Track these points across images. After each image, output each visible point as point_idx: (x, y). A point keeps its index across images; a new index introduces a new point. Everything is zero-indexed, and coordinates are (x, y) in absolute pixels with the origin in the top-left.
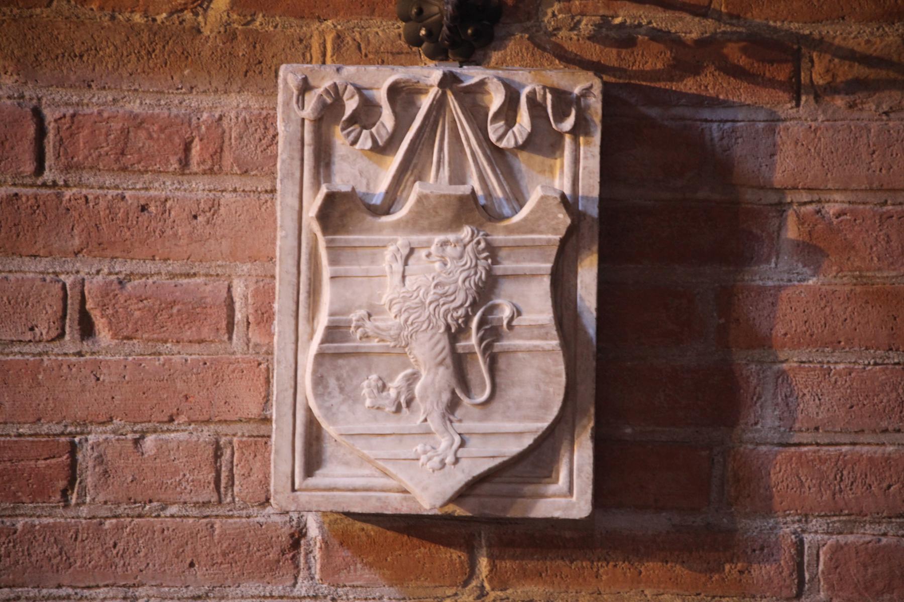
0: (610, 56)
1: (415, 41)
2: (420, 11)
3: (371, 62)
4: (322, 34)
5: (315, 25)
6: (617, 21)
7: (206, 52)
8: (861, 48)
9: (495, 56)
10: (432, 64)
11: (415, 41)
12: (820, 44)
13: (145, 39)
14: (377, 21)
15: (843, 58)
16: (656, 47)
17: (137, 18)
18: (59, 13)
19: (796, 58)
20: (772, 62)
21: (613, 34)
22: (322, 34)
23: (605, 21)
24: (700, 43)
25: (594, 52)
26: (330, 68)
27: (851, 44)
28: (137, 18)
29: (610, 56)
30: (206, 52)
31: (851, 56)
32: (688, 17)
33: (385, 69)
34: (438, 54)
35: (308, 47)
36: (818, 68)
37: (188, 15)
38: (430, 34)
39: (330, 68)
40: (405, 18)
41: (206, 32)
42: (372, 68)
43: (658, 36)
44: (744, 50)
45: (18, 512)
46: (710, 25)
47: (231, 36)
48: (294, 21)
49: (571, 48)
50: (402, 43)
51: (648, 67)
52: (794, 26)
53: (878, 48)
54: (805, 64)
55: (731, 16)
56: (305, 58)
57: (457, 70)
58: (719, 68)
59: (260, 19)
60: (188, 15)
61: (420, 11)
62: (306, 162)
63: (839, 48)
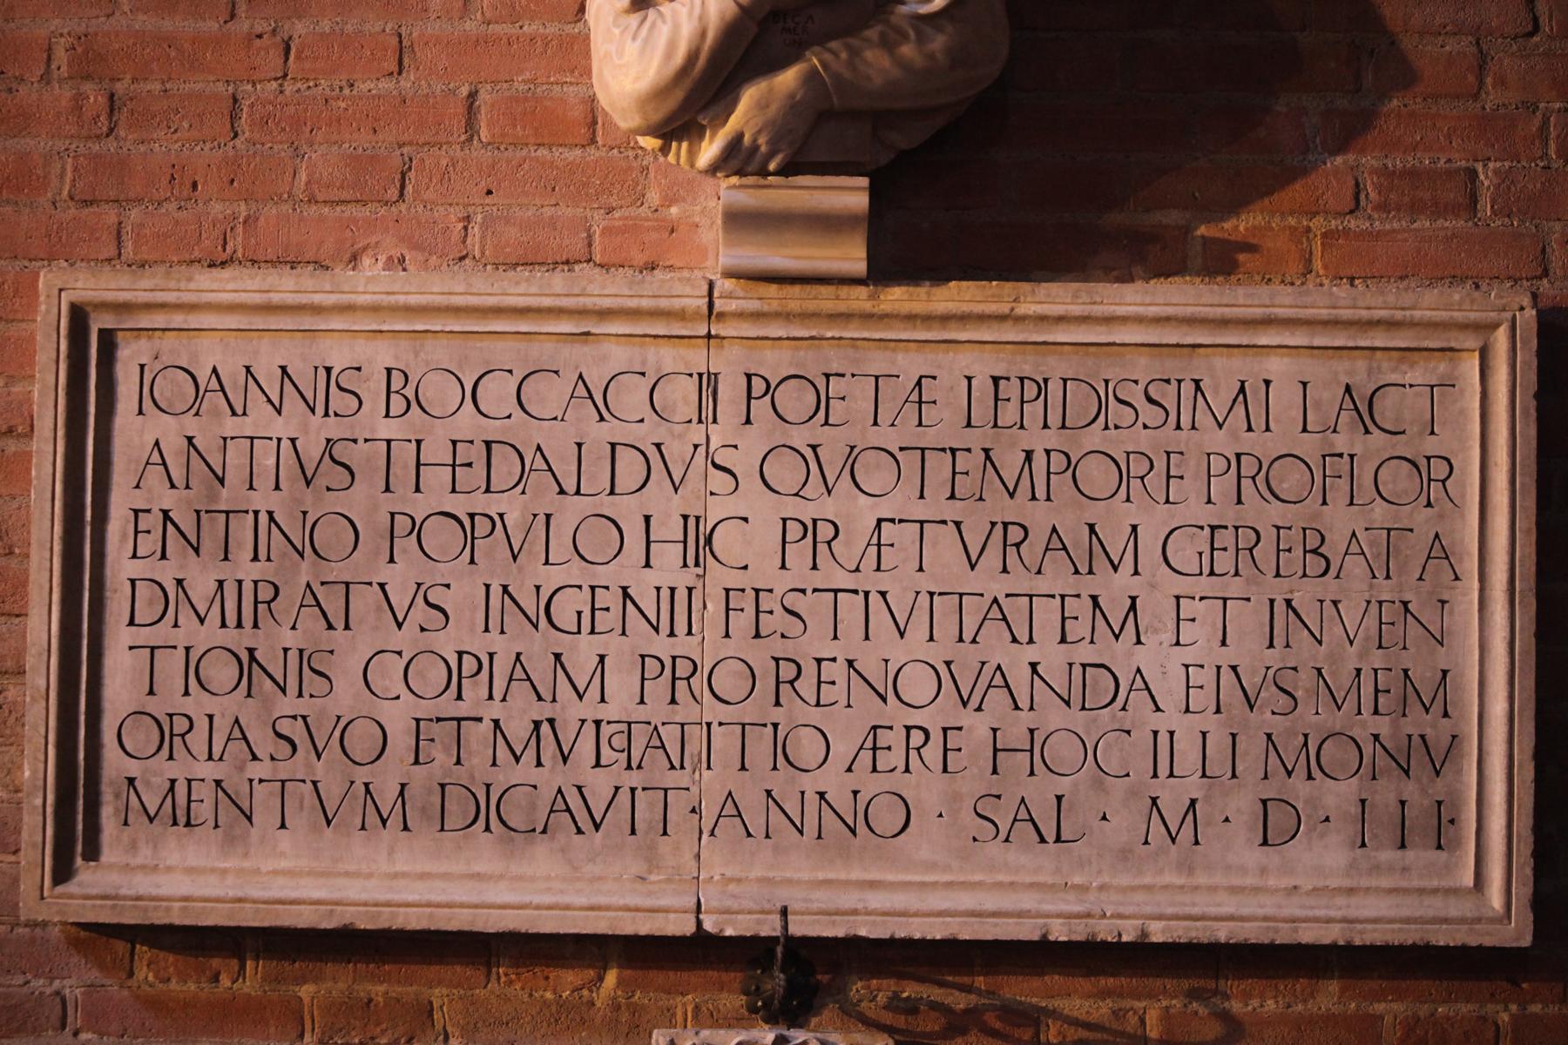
0: (900, 1021)
1: (753, 1010)
2: (758, 988)
3: (721, 1027)
4: (684, 1005)
5: (679, 998)
6: (905, 995)
7: (598, 1021)
8: (1083, 1017)
9: (814, 1021)
10: (766, 1027)
11: (753, 1010)
12: (1054, 1014)
13: (554, 1009)
14: (725, 995)
15: (1070, 1024)
16: (934, 1014)
17: (549, 995)
18: (492, 992)
19: (1037, 1024)
20: (1019, 1026)
21: (902, 1005)
22: (684, 1005)
23: (896, 996)
24: (966, 1011)
25: (888, 1018)
26: (690, 1032)
27: (1075, 1014)
28: (549, 995)
29: (900, 1021)
30: (598, 1021)
31: (1076, 1023)
32: (957, 993)
33: (732, 1032)
34: (771, 1020)
35: (674, 1015)
36: (1053, 1031)
37: (585, 992)
38: (765, 1004)
39: (690, 1032)
40: (746, 993)
41: (598, 1004)
42: (722, 1032)
43: (935, 1006)
44: (999, 1018)
45: (342, 867)
46: (973, 999)
47: (617, 1007)
48: (664, 996)
49: (871, 1014)
50: (744, 1011)
51: (928, 1029)
52: (1034, 1000)
53: (1094, 1017)
54: (1043, 1028)
55: (988, 992)
56: (672, 1025)
57: (786, 1033)
58: (981, 1031)
59: (638, 994)
60: (585, 992)
61: (758, 988)
62: (1050, 338)
63: (1067, 1016)
